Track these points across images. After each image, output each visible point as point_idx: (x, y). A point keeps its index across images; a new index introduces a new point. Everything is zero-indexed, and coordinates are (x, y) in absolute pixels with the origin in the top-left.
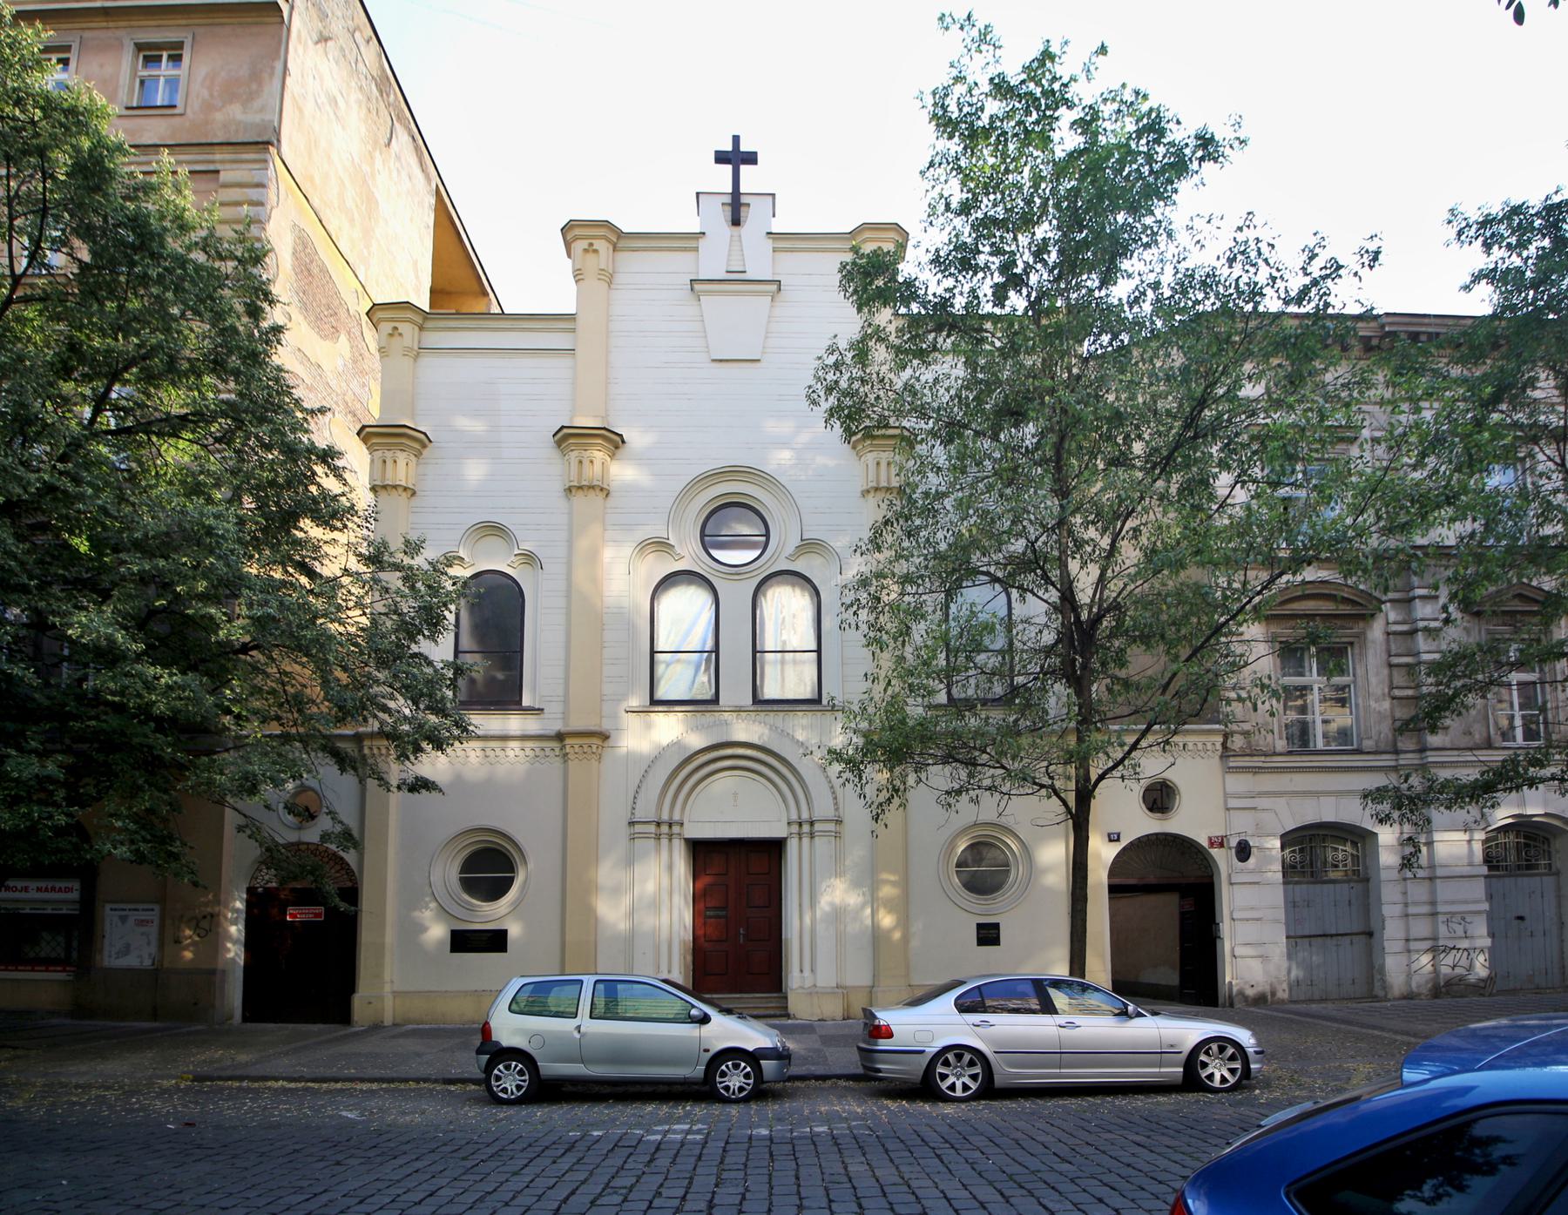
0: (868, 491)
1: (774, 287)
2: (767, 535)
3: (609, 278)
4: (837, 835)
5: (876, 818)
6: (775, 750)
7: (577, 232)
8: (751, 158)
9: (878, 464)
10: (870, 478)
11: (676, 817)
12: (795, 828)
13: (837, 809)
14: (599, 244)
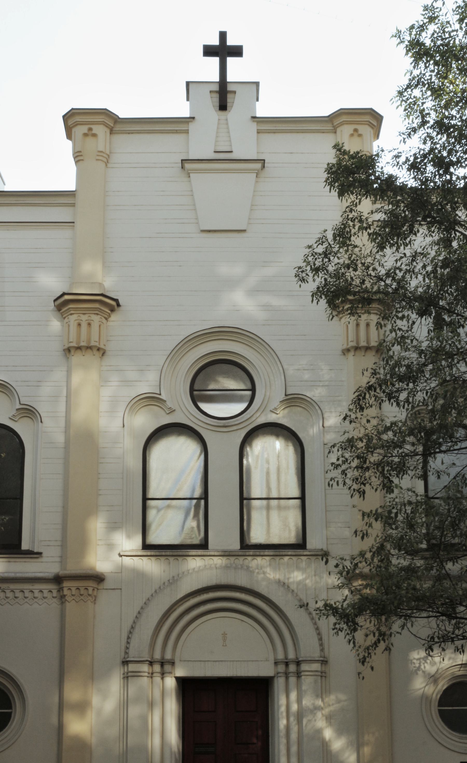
0: (348, 350)
1: (259, 165)
2: (253, 389)
5: (363, 661)
7: (78, 119)
10: (350, 339)
11: (168, 656)
12: (281, 668)
13: (322, 650)
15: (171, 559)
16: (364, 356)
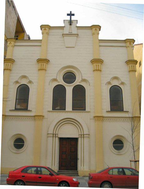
3: (48, 34)
4: (89, 137)
8: (73, 15)
9: (96, 66)
14: (46, 28)
15: (58, 112)
16: (140, 64)
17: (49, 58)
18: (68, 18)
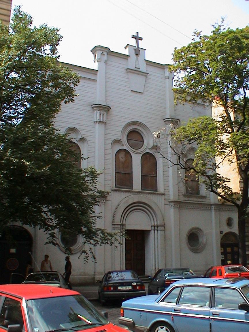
6: (127, 205)
8: (141, 39)
11: (124, 223)
12: (153, 228)
17: (109, 104)
18: (133, 42)
